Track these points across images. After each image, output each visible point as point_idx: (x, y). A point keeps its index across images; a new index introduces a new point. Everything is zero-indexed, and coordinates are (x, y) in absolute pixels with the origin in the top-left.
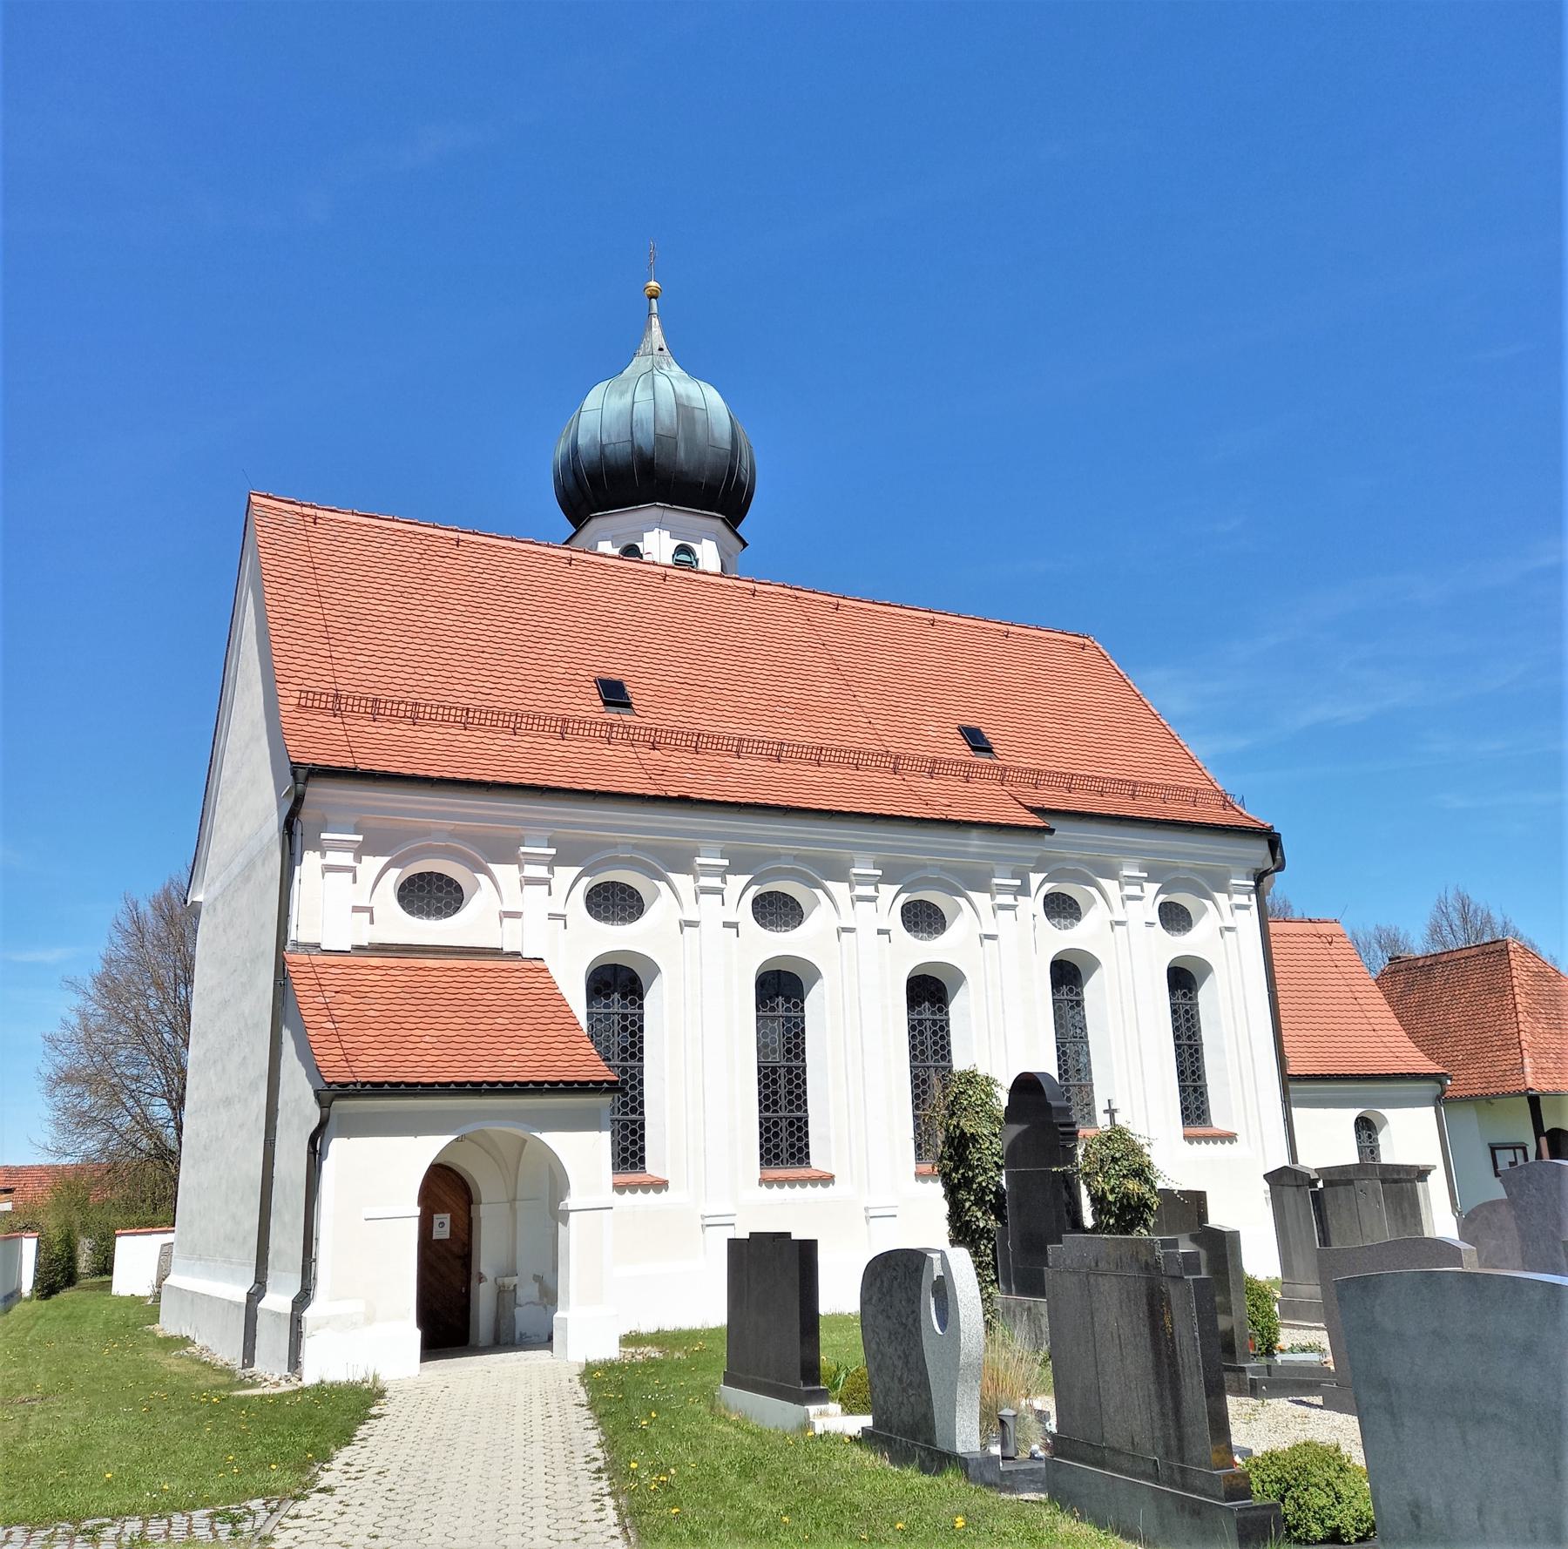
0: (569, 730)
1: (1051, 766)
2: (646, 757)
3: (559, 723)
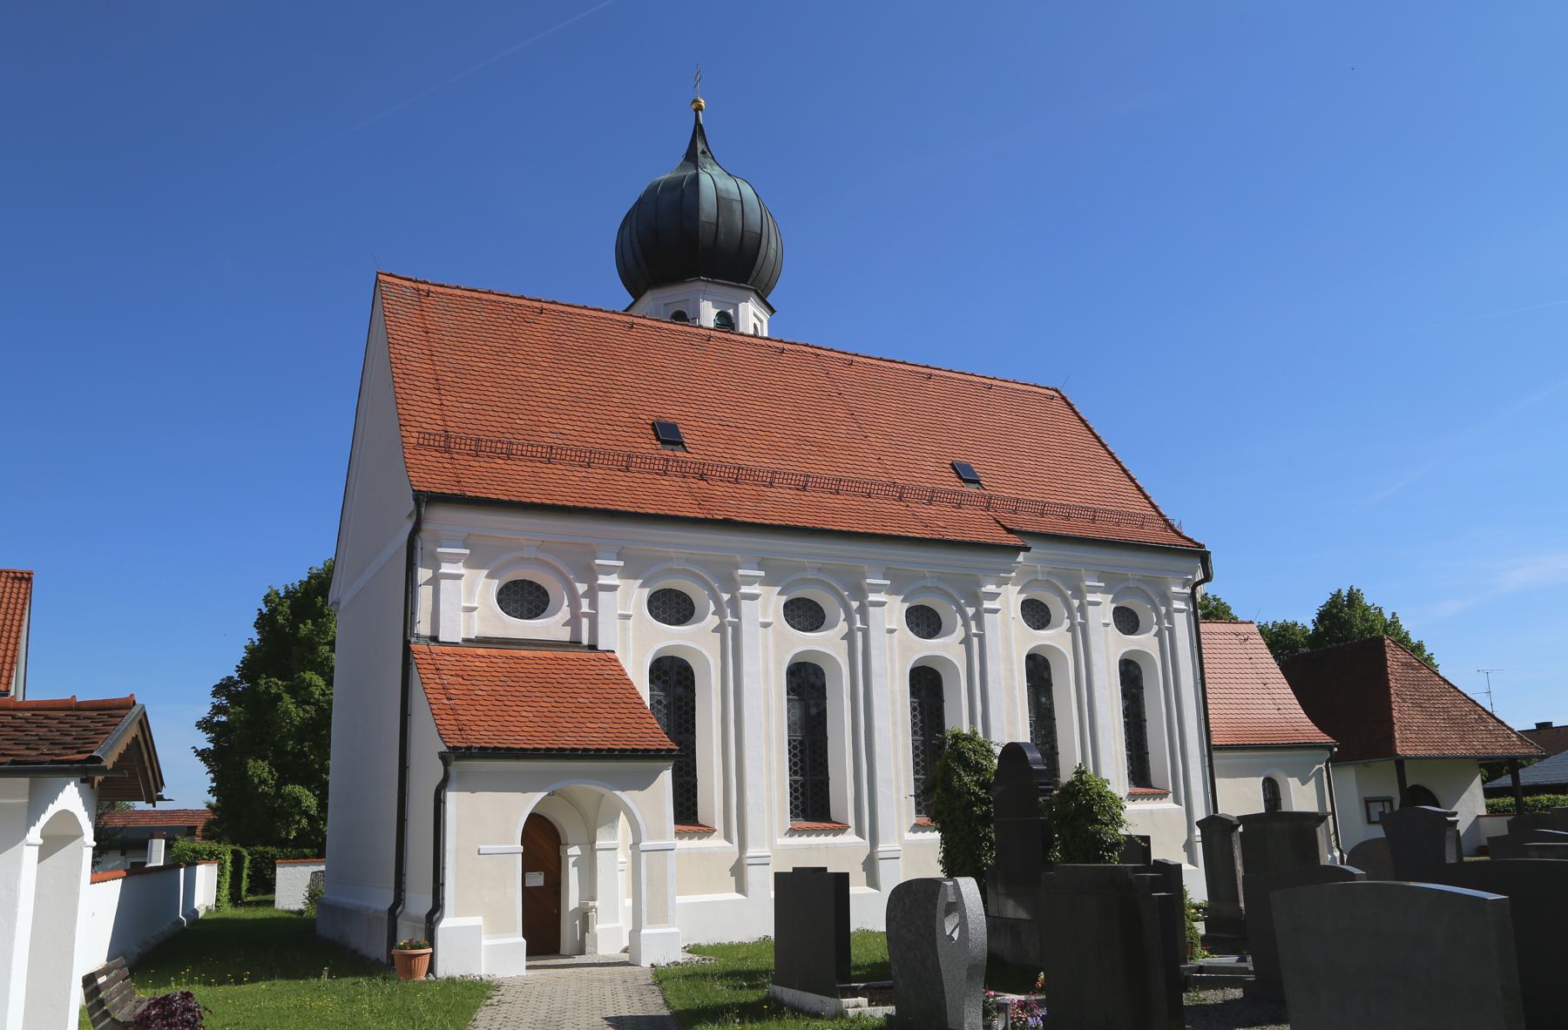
0: (633, 464)
1: (1027, 495)
2: (695, 486)
3: (625, 459)
